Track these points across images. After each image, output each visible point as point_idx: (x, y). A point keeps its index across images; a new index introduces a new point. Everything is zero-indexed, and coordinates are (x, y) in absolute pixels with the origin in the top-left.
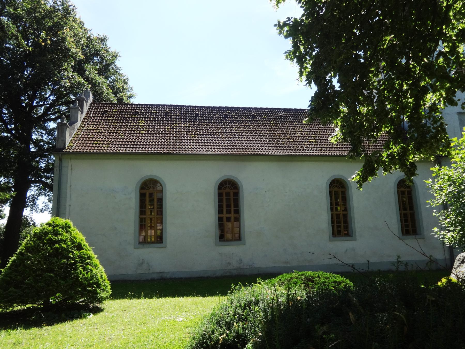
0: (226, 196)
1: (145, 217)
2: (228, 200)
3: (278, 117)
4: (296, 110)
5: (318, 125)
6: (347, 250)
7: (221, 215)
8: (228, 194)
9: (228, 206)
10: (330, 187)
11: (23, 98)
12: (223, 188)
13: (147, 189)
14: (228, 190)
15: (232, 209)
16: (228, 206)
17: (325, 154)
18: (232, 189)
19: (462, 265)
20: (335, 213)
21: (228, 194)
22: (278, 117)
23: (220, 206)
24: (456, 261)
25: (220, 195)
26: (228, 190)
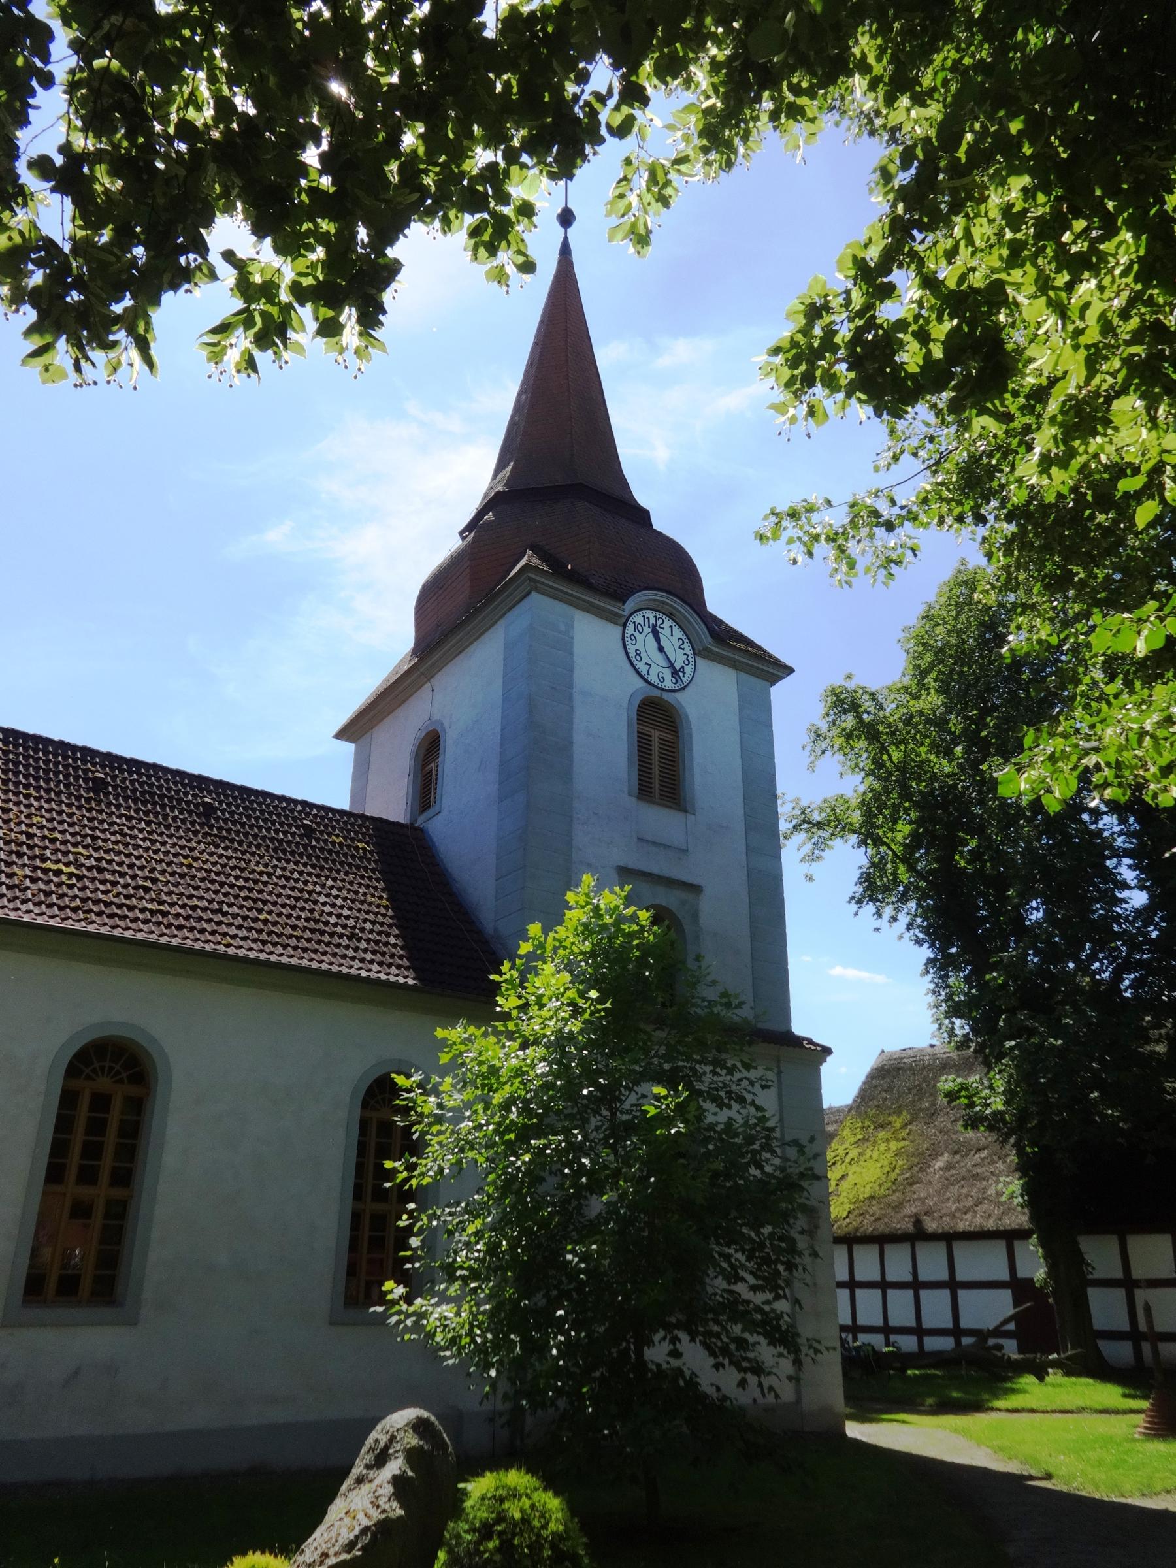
0: (92, 1108)
1: (369, 1199)
2: (97, 1127)
3: (297, 827)
4: (62, 745)
5: (129, 818)
6: (76, 1373)
7: (118, 1193)
8: (101, 1102)
9: (92, 1151)
10: (365, 1105)
11: (1036, 960)
12: (87, 1071)
13: (88, 1077)
14: (104, 1083)
15: (107, 1163)
16: (92, 1151)
17: (335, 968)
18: (121, 1081)
19: (372, 1474)
20: (101, 1192)
21: (101, 1102)
22: (197, 806)
23: (59, 1148)
24: (362, 1452)
25: (68, 1099)
26: (104, 1083)
